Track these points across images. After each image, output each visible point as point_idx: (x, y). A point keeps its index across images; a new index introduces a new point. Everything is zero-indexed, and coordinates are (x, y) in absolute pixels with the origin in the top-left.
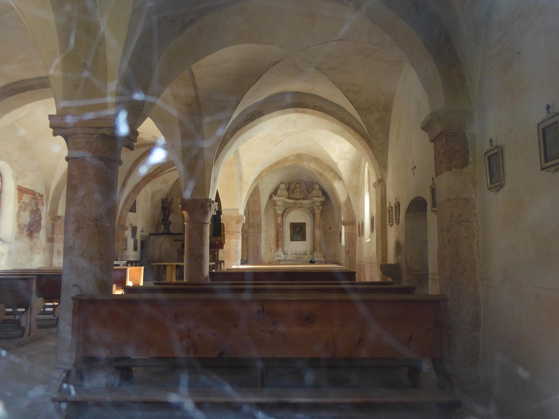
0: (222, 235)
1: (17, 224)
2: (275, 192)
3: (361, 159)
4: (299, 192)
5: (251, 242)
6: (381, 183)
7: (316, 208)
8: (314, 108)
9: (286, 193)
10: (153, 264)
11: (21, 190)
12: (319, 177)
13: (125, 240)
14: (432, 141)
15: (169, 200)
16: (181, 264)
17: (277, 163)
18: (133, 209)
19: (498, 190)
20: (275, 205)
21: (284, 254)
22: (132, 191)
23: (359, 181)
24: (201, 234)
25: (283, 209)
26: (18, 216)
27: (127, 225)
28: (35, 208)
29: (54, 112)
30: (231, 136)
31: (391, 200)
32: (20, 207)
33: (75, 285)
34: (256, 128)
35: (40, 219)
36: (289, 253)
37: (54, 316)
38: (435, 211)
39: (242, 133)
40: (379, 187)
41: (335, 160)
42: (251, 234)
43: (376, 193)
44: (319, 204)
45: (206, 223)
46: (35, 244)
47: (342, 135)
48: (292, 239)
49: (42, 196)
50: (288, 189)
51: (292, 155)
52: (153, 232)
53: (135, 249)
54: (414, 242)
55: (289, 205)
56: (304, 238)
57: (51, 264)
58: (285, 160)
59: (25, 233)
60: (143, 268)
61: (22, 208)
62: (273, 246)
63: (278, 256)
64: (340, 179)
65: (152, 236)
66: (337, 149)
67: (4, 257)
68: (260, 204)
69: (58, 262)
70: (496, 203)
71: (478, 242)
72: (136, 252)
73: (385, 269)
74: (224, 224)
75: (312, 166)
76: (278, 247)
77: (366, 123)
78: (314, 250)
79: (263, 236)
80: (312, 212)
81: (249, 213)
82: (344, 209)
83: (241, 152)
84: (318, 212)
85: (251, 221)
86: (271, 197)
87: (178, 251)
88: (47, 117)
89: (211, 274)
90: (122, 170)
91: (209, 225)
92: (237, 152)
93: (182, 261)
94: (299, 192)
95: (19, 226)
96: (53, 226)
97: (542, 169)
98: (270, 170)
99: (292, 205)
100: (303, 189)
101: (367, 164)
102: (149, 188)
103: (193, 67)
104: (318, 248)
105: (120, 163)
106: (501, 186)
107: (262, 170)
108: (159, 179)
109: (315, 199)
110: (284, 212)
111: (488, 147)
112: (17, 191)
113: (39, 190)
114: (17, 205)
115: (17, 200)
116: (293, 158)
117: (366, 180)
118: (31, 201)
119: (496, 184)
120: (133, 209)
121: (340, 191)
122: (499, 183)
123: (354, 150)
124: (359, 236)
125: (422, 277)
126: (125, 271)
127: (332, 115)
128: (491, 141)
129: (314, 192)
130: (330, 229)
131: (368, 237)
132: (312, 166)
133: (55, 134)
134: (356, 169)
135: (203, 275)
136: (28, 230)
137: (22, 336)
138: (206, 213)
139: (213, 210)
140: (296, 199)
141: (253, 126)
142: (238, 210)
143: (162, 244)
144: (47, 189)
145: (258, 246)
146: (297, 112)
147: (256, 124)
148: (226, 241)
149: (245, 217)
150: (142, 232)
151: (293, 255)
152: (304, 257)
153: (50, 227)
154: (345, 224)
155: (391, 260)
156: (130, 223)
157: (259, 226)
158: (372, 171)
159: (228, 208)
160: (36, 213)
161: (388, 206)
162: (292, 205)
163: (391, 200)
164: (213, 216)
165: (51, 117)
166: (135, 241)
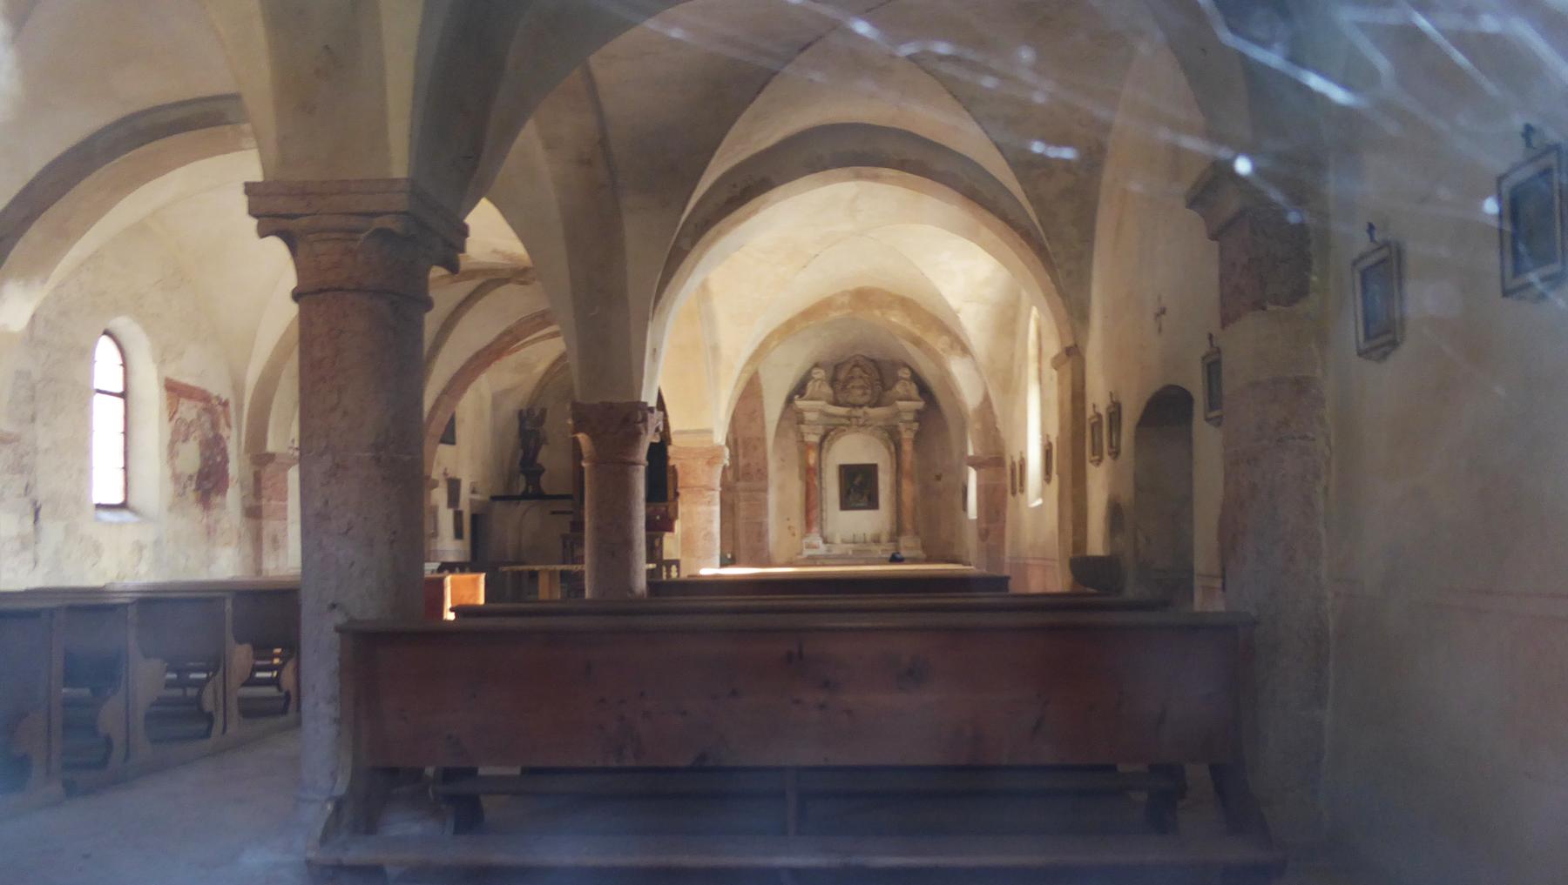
0: (671, 494)
1: (168, 473)
2: (800, 390)
3: (1019, 297)
4: (862, 387)
5: (743, 510)
6: (1072, 355)
7: (902, 427)
8: (902, 165)
9: (827, 390)
10: (505, 569)
11: (175, 391)
12: (911, 348)
13: (434, 511)
14: (1213, 237)
15: (537, 413)
16: (574, 568)
17: (807, 314)
18: (449, 437)
19: (1385, 356)
20: (801, 421)
21: (825, 542)
22: (445, 392)
23: (1012, 356)
24: (626, 489)
25: (821, 430)
26: (172, 452)
27: (436, 474)
28: (211, 435)
29: (256, 175)
30: (693, 244)
31: (1098, 397)
32: (175, 432)
33: (334, 606)
34: (755, 220)
35: (226, 461)
36: (838, 540)
37: (280, 689)
38: (1220, 417)
39: (720, 234)
40: (1067, 367)
41: (954, 302)
42: (742, 494)
43: (1060, 383)
44: (910, 417)
45: (634, 464)
46: (217, 521)
47: (972, 236)
48: (845, 505)
49: (225, 404)
50: (833, 381)
51: (844, 293)
52: (500, 493)
53: (458, 534)
54: (1154, 505)
55: (835, 421)
56: (873, 504)
57: (259, 571)
58: (825, 305)
59: (191, 495)
60: (482, 577)
61: (178, 436)
62: (797, 521)
63: (809, 547)
64: (965, 350)
65: (498, 503)
66: (960, 274)
67: (147, 554)
68: (763, 417)
69: (286, 560)
70: (1383, 386)
71: (1326, 489)
72: (459, 542)
73: (1082, 565)
74: (678, 467)
75: (893, 319)
76: (808, 524)
77: (1036, 201)
78: (897, 531)
79: (772, 497)
80: (892, 437)
81: (736, 441)
82: (973, 428)
83: (715, 286)
84: (907, 436)
85: (742, 462)
86: (790, 400)
87: (564, 537)
88: (242, 189)
89: (649, 584)
90: (431, 323)
91: (642, 469)
92: (704, 287)
93: (580, 560)
94: (862, 387)
95: (176, 478)
96: (258, 479)
97: (1506, 293)
98: (787, 330)
99: (844, 421)
100: (874, 376)
101: (1034, 311)
102: (484, 387)
103: (594, 60)
104: (908, 526)
105: (428, 305)
106: (1394, 344)
107: (768, 331)
108: (510, 360)
109: (902, 404)
110: (824, 438)
111: (1362, 243)
112: (165, 394)
113: (218, 387)
114: (168, 428)
115: (166, 417)
116: (846, 299)
117: (1032, 351)
118: (199, 417)
119: (1378, 342)
120: (449, 437)
121: (966, 383)
122: (1390, 337)
123: (1003, 274)
124: (1014, 493)
125: (1179, 583)
126: (439, 584)
127: (949, 185)
128: (1371, 228)
129: (899, 389)
130: (939, 478)
131: (1036, 495)
132: (896, 318)
133: (263, 233)
134: (1007, 324)
135: (631, 591)
136: (197, 489)
137: (207, 735)
138: (635, 436)
139: (651, 430)
140: (854, 406)
141: (748, 216)
142: (709, 432)
143: (520, 524)
144: (238, 387)
145: (761, 524)
146: (858, 177)
147: (755, 211)
148: (681, 509)
149: (727, 452)
150: (474, 491)
151: (850, 540)
152: (874, 547)
153: (251, 480)
154: (976, 463)
155: (1096, 545)
156: (441, 470)
157: (762, 474)
158: (1050, 327)
159: (686, 428)
160: (213, 450)
161: (1090, 412)
162: (844, 421)
163: (1098, 397)
164: (652, 444)
165: (250, 189)
166: (458, 516)
